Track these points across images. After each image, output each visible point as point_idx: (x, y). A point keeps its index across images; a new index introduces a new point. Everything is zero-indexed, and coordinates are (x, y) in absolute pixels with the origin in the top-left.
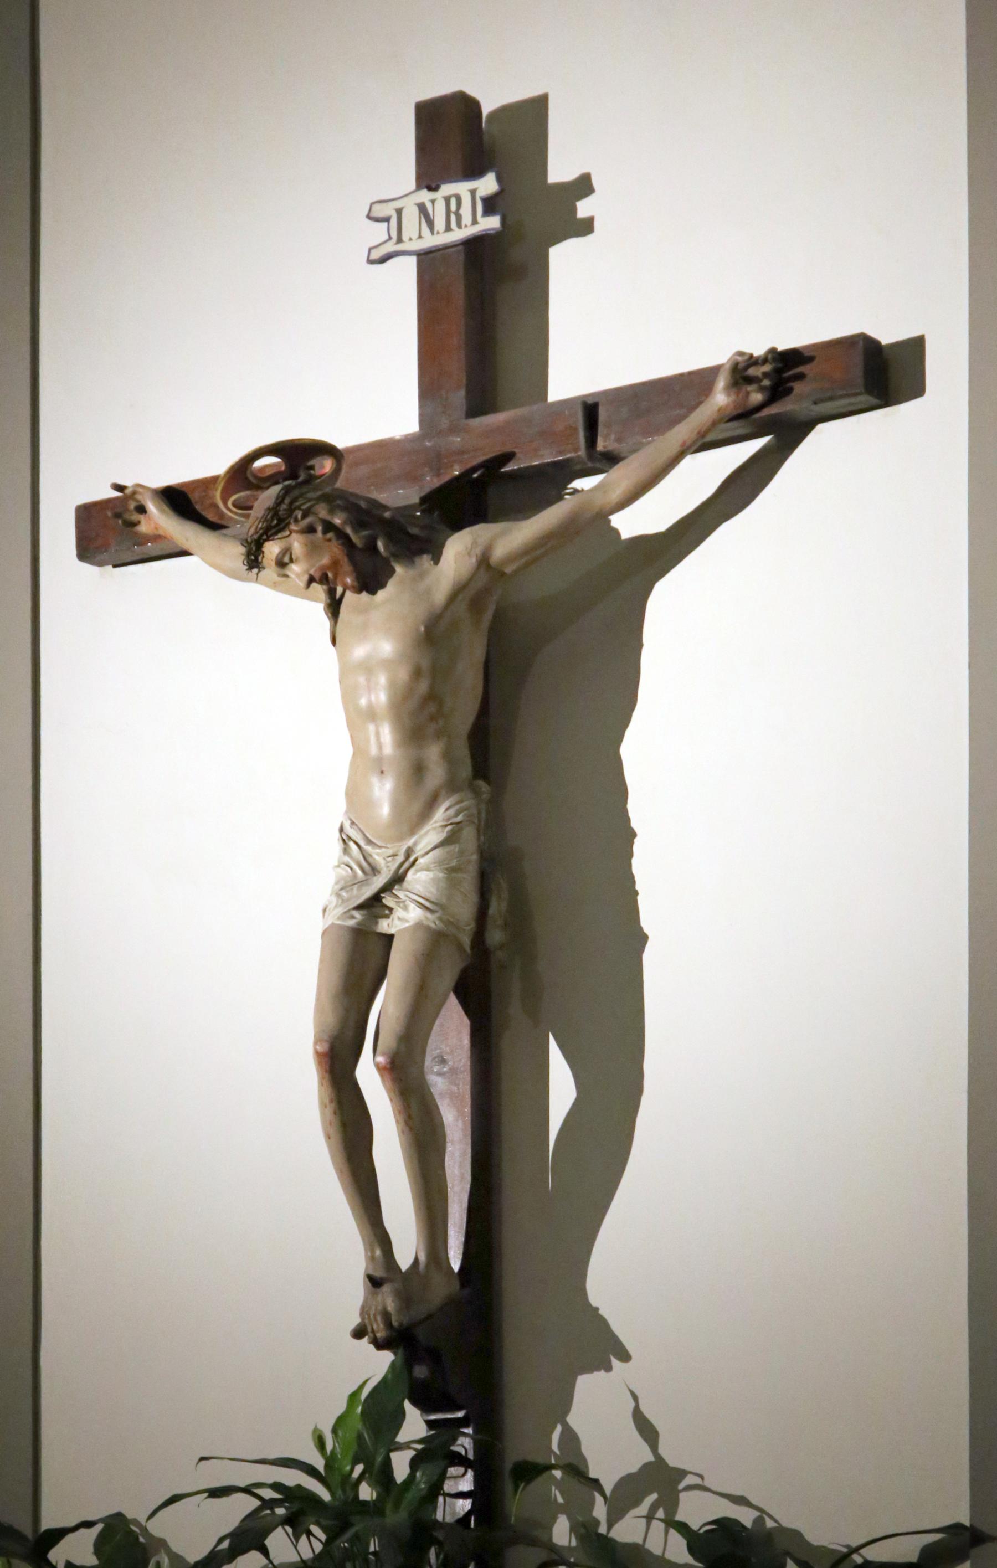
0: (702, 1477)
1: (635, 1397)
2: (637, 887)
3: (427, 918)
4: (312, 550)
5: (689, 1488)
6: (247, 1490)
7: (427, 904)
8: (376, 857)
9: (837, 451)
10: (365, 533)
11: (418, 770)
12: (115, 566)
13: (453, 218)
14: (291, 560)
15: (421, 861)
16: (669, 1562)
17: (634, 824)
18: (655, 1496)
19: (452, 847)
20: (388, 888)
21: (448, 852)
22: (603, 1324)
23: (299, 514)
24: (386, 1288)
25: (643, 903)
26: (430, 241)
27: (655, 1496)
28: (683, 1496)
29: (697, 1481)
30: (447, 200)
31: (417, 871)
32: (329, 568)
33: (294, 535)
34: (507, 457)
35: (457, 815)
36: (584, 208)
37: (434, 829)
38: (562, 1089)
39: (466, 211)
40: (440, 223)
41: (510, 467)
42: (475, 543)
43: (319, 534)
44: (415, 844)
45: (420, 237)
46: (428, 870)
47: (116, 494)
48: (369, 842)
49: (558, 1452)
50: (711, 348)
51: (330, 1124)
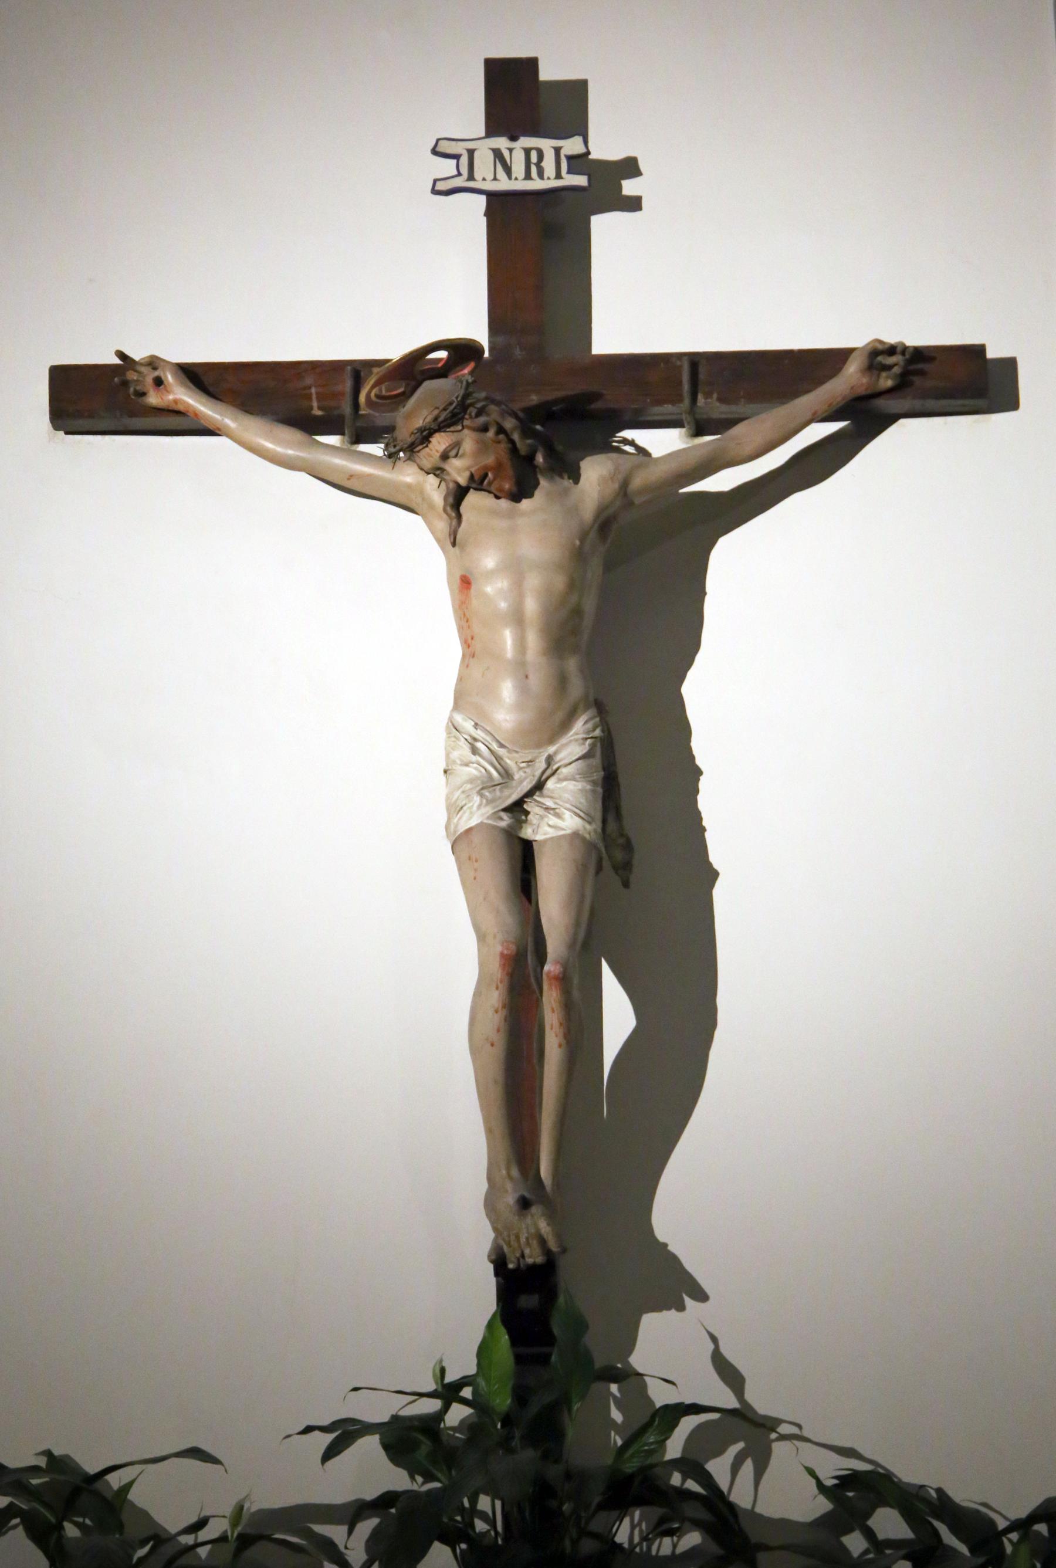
0: (799, 1426)
1: (714, 1339)
2: (704, 823)
3: (585, 829)
4: (482, 448)
5: (783, 1437)
6: (323, 1429)
7: (582, 814)
8: (508, 761)
9: (911, 444)
10: (529, 441)
11: (562, 682)
12: (67, 433)
13: (534, 169)
14: (456, 456)
15: (564, 771)
16: (760, 1516)
17: (699, 762)
18: (740, 1445)
19: (591, 760)
20: (530, 794)
21: (588, 765)
22: (674, 1260)
23: (473, 411)
24: (535, 1210)
25: (712, 839)
26: (504, 184)
27: (740, 1445)
28: (775, 1446)
29: (794, 1430)
30: (527, 152)
31: (560, 780)
32: (491, 469)
33: (466, 431)
34: (595, 397)
35: (594, 730)
36: (629, 187)
37: (576, 740)
38: (618, 1017)
39: (549, 164)
40: (518, 169)
41: (597, 405)
42: (616, 469)
43: (491, 434)
44: (556, 753)
45: (495, 179)
46: (574, 779)
47: (117, 361)
48: (502, 746)
49: (618, 1395)
50: (850, 331)
51: (498, 1031)
